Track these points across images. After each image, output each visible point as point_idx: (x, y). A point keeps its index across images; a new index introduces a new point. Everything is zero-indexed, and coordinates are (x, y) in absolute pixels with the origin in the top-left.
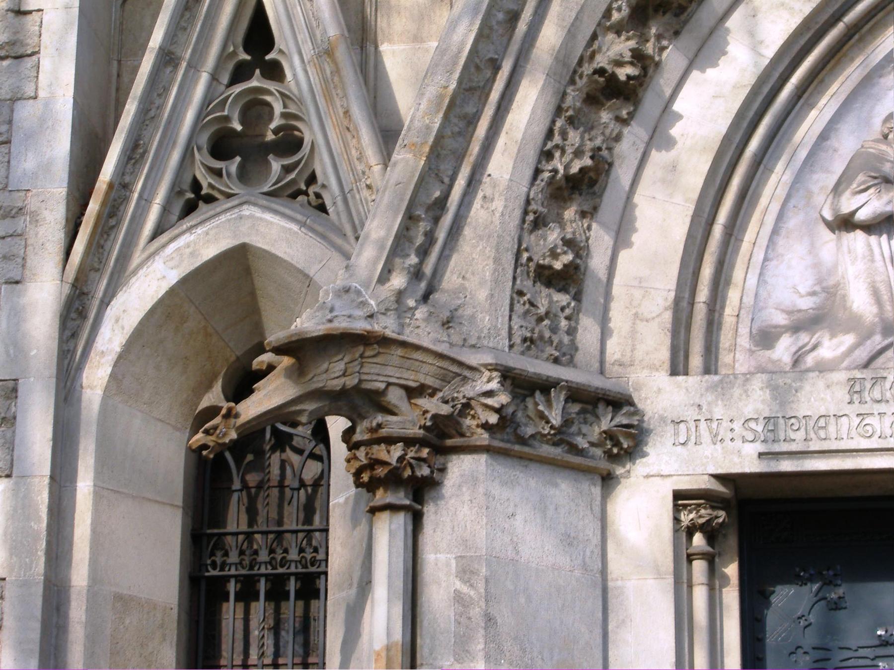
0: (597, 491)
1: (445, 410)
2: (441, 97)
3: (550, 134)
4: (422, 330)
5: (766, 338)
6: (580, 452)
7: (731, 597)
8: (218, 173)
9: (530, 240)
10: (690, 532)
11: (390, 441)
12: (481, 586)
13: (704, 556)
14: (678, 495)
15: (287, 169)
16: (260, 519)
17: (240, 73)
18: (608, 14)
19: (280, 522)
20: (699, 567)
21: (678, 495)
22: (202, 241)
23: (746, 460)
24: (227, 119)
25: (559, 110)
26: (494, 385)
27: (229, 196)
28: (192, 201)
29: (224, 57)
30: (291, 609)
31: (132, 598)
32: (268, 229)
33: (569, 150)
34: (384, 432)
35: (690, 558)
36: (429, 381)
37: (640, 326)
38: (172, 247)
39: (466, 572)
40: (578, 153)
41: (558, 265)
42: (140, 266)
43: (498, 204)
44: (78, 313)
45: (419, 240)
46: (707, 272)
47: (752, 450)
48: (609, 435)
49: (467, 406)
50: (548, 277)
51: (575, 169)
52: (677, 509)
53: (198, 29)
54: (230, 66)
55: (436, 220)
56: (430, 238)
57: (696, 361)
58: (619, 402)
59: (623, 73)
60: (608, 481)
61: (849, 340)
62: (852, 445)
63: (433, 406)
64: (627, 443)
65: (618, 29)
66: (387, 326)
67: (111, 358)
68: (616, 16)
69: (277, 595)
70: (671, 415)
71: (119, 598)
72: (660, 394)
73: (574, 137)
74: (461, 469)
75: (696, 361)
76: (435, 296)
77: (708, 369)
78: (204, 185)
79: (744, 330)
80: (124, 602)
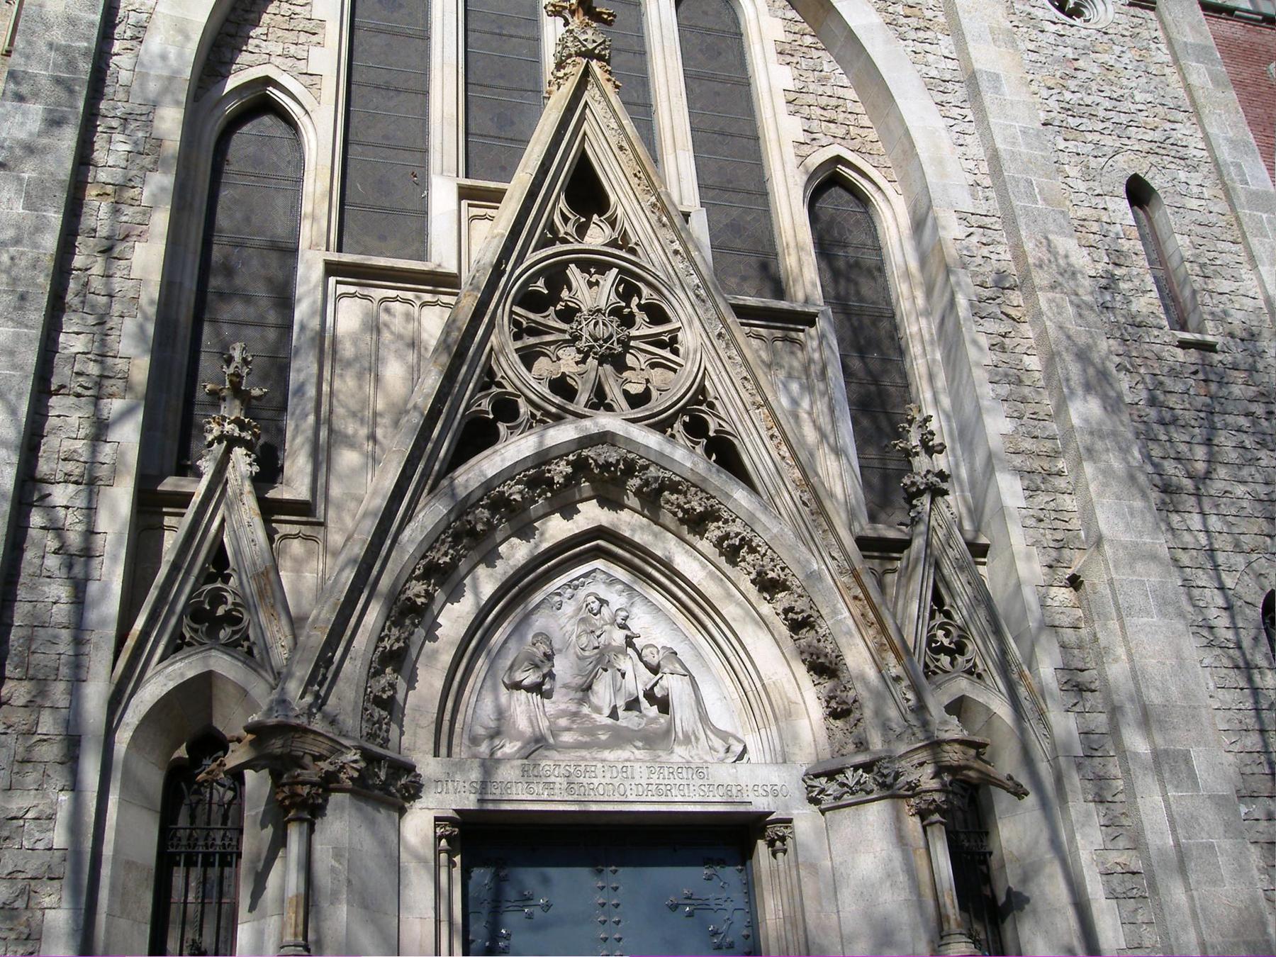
0: (396, 815)
1: (332, 768)
2: (336, 604)
3: (383, 630)
4: (318, 725)
5: (475, 741)
6: (392, 795)
7: (457, 873)
8: (196, 631)
9: (372, 682)
10: (440, 838)
11: (304, 783)
12: (346, 863)
13: (447, 851)
14: (437, 819)
15: (234, 633)
16: (197, 821)
17: (210, 579)
18: (413, 571)
19: (209, 823)
20: (443, 856)
21: (437, 819)
22: (184, 668)
23: (470, 803)
24: (203, 602)
25: (388, 618)
26: (357, 757)
27: (202, 644)
28: (177, 646)
29: (203, 568)
30: (214, 873)
31: (133, 862)
32: (223, 664)
33: (393, 638)
34: (301, 778)
35: (440, 852)
36: (325, 753)
37: (419, 730)
38: (171, 668)
39: (338, 855)
40: (398, 640)
41: (385, 696)
42: (151, 677)
43: (358, 663)
44: (117, 702)
45: (320, 677)
46: (450, 704)
47: (473, 797)
48: (405, 787)
49: (343, 767)
50: (378, 702)
51: (395, 647)
52: (436, 826)
53: (531, 576)
54: (205, 575)
55: (327, 668)
56: (325, 678)
57: (443, 750)
58: (410, 769)
59: (420, 601)
60: (402, 811)
61: (519, 744)
62: (519, 797)
63: (325, 766)
64: (414, 791)
65: (418, 579)
66: (303, 721)
67: (133, 727)
68: (417, 572)
69: (207, 864)
70: (433, 778)
71: (127, 862)
72: (427, 766)
73: (395, 631)
74: (335, 798)
75: (443, 750)
76: (325, 708)
77: (449, 755)
78: (188, 636)
79: (465, 736)
80: (130, 865)
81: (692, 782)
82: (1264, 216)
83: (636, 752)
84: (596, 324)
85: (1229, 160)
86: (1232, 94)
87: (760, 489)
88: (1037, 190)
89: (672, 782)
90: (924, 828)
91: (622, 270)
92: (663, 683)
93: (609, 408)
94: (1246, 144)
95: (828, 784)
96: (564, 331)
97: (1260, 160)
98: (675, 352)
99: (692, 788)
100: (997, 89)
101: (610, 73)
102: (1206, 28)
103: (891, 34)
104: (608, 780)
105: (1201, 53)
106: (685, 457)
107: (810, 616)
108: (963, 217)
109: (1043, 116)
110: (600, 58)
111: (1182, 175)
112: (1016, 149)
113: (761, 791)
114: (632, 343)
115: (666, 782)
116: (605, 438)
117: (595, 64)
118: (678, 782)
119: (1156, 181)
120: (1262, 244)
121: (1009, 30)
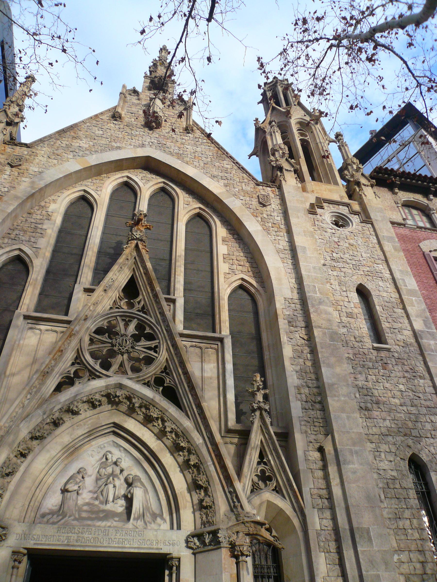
14: (13, 552)
21: (13, 552)
81: (135, 538)
82: (414, 298)
83: (115, 523)
85: (399, 277)
86: (402, 254)
87: (183, 408)
88: (317, 289)
89: (126, 537)
90: (237, 563)
91: (120, 316)
94: (407, 272)
97: (412, 277)
98: (156, 352)
99: (135, 541)
100: (304, 252)
101: (145, 246)
102: (392, 230)
103: (265, 233)
104: (96, 536)
105: (390, 239)
109: (323, 262)
110: (141, 240)
111: (381, 283)
112: (310, 274)
113: (167, 543)
114: (136, 348)
115: (123, 537)
117: (139, 242)
119: (370, 286)
120: (412, 309)
121: (311, 231)
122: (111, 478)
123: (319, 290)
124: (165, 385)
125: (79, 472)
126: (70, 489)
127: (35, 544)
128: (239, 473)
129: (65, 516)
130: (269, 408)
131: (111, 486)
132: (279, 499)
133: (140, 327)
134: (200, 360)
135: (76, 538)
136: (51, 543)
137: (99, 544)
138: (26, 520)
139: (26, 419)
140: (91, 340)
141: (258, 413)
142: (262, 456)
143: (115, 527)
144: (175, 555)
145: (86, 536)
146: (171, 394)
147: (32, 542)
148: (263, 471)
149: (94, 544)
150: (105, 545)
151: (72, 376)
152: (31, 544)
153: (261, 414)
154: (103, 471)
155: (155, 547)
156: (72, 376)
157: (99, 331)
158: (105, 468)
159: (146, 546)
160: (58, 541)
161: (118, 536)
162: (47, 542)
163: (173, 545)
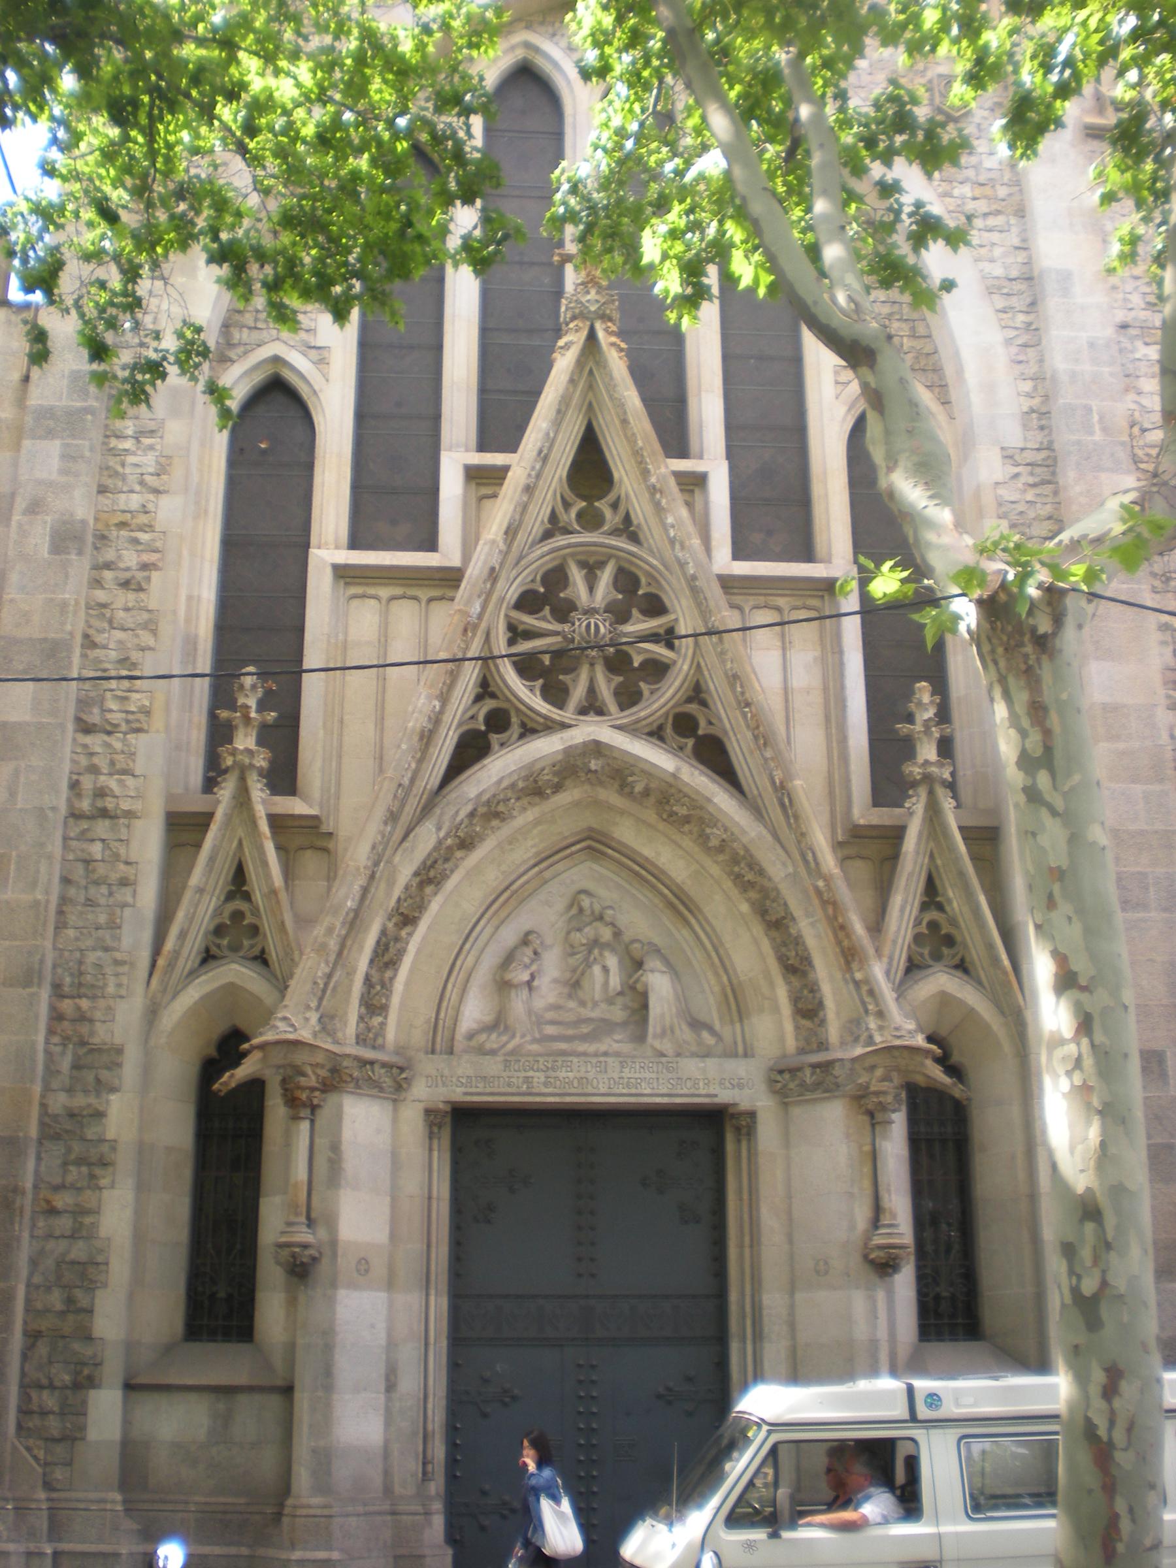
84: (589, 625)
88: (1096, 418)
89: (642, 1075)
92: (643, 979)
93: (600, 712)
95: (799, 1080)
96: (557, 633)
98: (670, 646)
100: (1066, 291)
104: (582, 1074)
106: (659, 758)
107: (784, 918)
108: (1008, 457)
116: (597, 748)
118: (648, 1075)
122: (596, 951)
123: (1101, 419)
124: (700, 732)
125: (525, 941)
126: (515, 981)
127: (466, 1094)
128: (876, 927)
129: (513, 1036)
130: (953, 774)
131: (597, 970)
132: (969, 988)
133: (627, 580)
134: (779, 644)
135: (543, 1079)
136: (496, 1090)
137: (590, 1090)
138: (438, 1047)
139: (406, 844)
140: (512, 628)
141: (923, 792)
142: (931, 887)
143: (617, 1054)
144: (745, 1105)
145: (562, 1074)
146: (714, 755)
147: (459, 1090)
148: (933, 926)
149: (580, 1091)
150: (602, 1090)
151: (483, 728)
152: (458, 1094)
153: (931, 793)
154: (577, 937)
155: (703, 1092)
156: (483, 728)
157: (528, 602)
158: (579, 930)
159: (685, 1091)
160: (509, 1085)
161: (626, 1073)
162: (488, 1090)
163: (740, 1086)
